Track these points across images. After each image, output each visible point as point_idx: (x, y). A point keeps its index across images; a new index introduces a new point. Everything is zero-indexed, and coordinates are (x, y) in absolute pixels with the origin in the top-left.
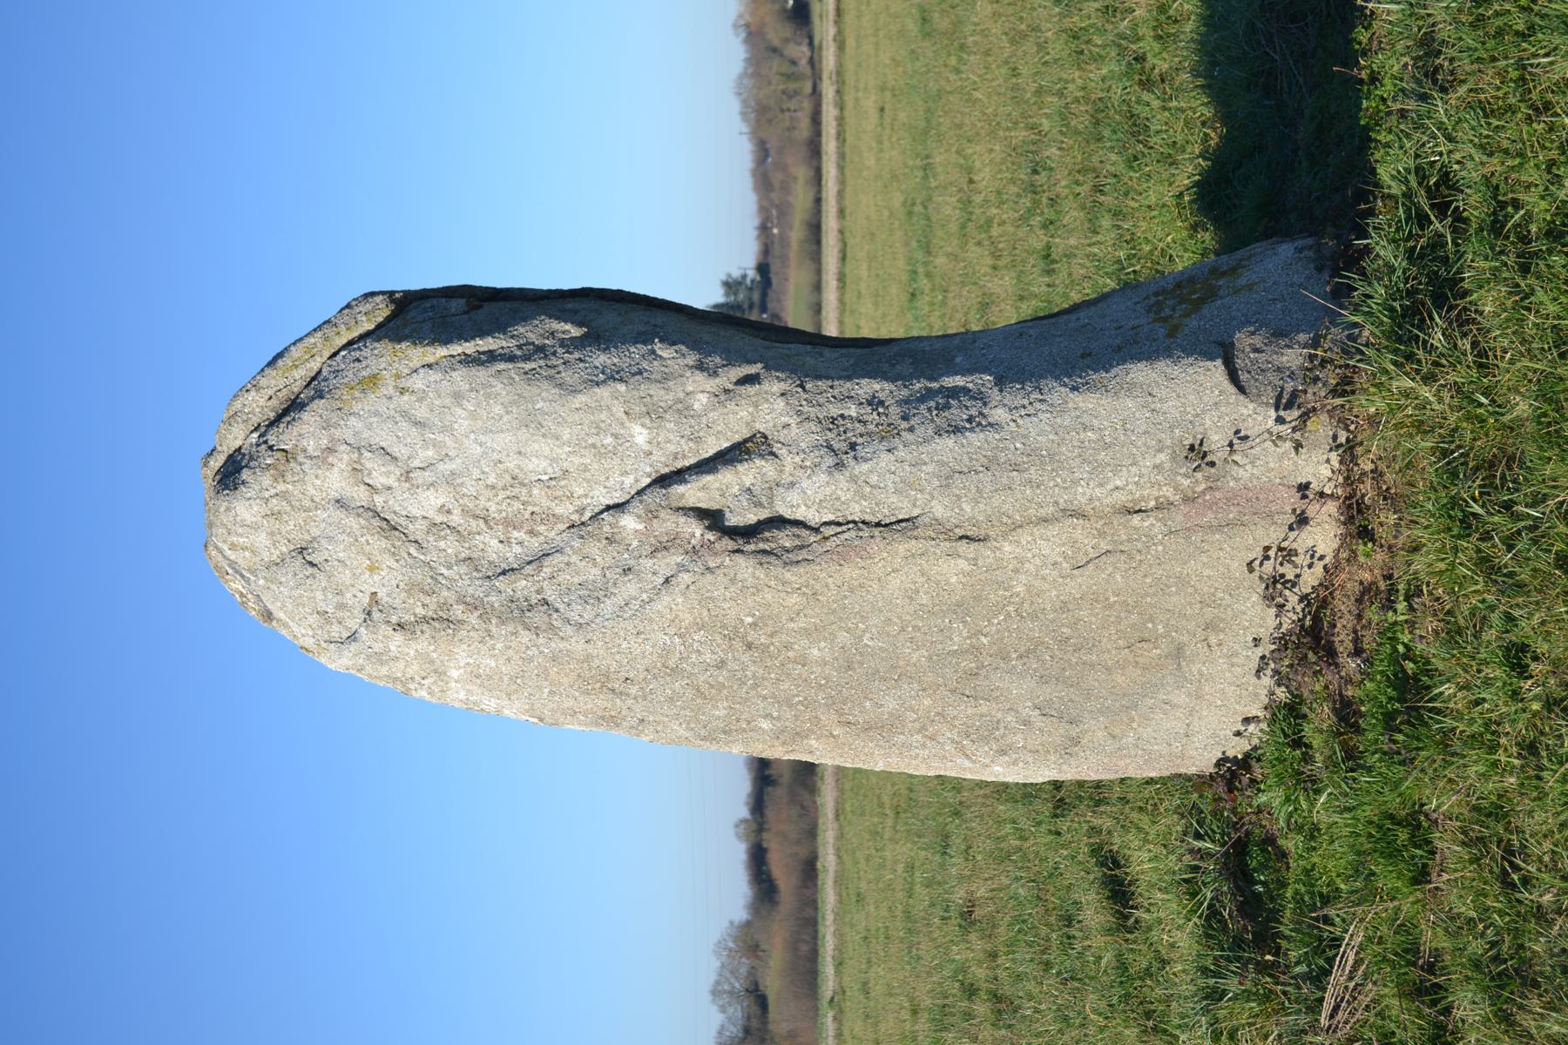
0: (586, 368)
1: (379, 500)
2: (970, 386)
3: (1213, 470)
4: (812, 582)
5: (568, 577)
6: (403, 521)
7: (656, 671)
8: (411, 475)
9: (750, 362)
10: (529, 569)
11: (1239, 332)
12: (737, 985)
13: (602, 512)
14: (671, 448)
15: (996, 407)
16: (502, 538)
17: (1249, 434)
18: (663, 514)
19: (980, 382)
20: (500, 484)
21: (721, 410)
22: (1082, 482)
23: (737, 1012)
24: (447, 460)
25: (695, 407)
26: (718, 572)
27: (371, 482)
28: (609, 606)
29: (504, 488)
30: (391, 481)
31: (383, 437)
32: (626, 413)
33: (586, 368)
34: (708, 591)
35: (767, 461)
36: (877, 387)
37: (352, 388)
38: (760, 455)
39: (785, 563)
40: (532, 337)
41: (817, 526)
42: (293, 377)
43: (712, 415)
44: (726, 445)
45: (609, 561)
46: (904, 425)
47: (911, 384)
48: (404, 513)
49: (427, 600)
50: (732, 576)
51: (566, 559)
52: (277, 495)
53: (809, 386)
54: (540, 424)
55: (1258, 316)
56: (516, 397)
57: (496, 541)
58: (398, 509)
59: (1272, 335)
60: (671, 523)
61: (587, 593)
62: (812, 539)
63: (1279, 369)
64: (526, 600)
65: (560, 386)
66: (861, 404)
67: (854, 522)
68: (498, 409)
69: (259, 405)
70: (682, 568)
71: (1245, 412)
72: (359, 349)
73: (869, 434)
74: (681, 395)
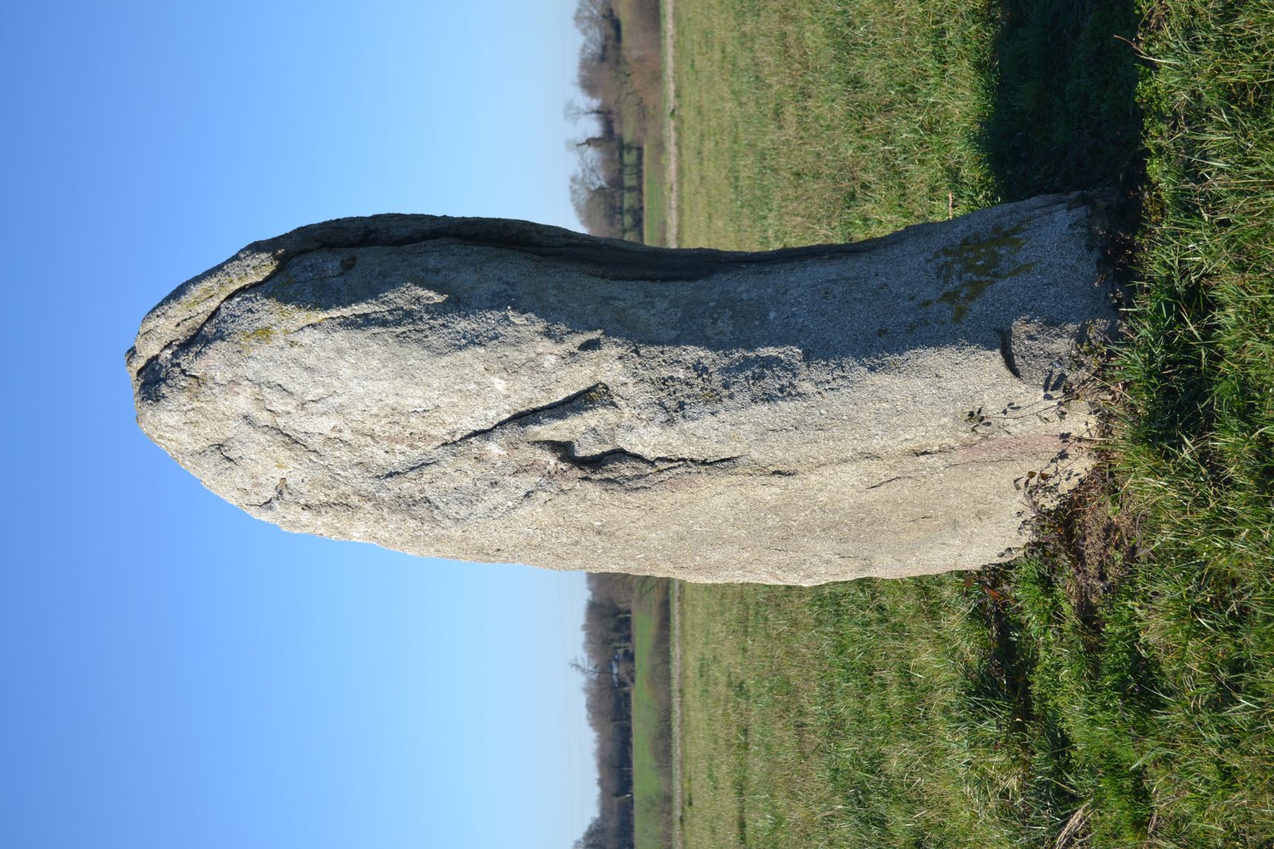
0: (450, 333)
1: (281, 422)
2: (782, 356)
3: (989, 428)
4: (649, 503)
5: (444, 483)
6: (301, 436)
7: (522, 547)
8: (306, 406)
9: (591, 329)
10: (412, 474)
11: (1017, 320)
12: (595, 12)
13: (470, 436)
14: (526, 394)
15: (803, 380)
16: (387, 449)
17: (1021, 405)
18: (521, 446)
19: (790, 353)
20: (382, 414)
21: (568, 369)
22: (877, 437)
23: (596, 33)
24: (335, 395)
25: (545, 365)
26: (570, 493)
27: (272, 409)
28: (480, 508)
29: (387, 416)
30: (289, 408)
31: (279, 376)
32: (486, 369)
33: (450, 333)
34: (563, 505)
35: (608, 410)
36: (702, 354)
37: (248, 337)
38: (603, 405)
39: (627, 490)
40: (401, 303)
41: (653, 460)
42: (197, 307)
43: (560, 373)
44: (572, 392)
45: (478, 474)
46: (725, 392)
47: (731, 354)
48: (303, 431)
49: (328, 492)
50: (583, 496)
51: (443, 470)
52: (193, 409)
53: (642, 352)
54: (412, 375)
55: (1034, 303)
56: (391, 356)
57: (382, 452)
58: (297, 428)
59: (1045, 323)
60: (528, 453)
61: (462, 496)
62: (649, 471)
63: (1049, 356)
64: (411, 497)
65: (428, 348)
66: (688, 368)
67: (684, 460)
68: (375, 363)
69: (170, 326)
70: (539, 487)
71: (1018, 391)
72: (250, 299)
73: (695, 396)
74: (533, 355)
